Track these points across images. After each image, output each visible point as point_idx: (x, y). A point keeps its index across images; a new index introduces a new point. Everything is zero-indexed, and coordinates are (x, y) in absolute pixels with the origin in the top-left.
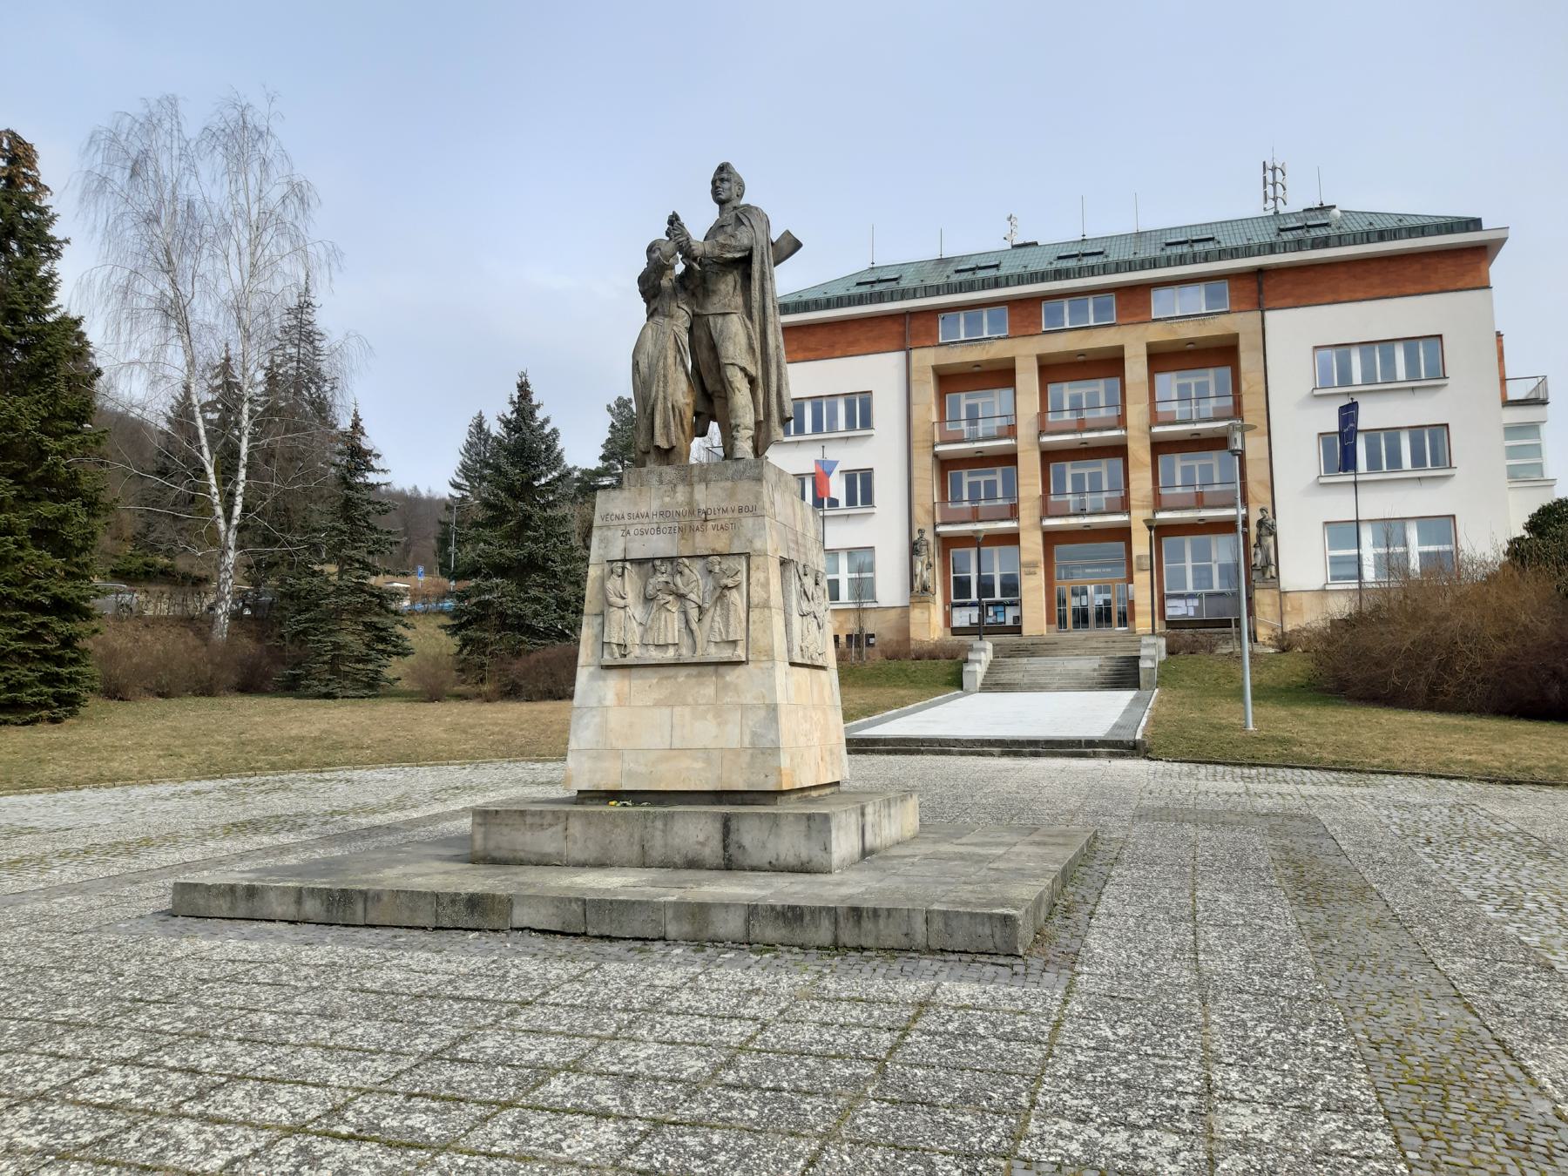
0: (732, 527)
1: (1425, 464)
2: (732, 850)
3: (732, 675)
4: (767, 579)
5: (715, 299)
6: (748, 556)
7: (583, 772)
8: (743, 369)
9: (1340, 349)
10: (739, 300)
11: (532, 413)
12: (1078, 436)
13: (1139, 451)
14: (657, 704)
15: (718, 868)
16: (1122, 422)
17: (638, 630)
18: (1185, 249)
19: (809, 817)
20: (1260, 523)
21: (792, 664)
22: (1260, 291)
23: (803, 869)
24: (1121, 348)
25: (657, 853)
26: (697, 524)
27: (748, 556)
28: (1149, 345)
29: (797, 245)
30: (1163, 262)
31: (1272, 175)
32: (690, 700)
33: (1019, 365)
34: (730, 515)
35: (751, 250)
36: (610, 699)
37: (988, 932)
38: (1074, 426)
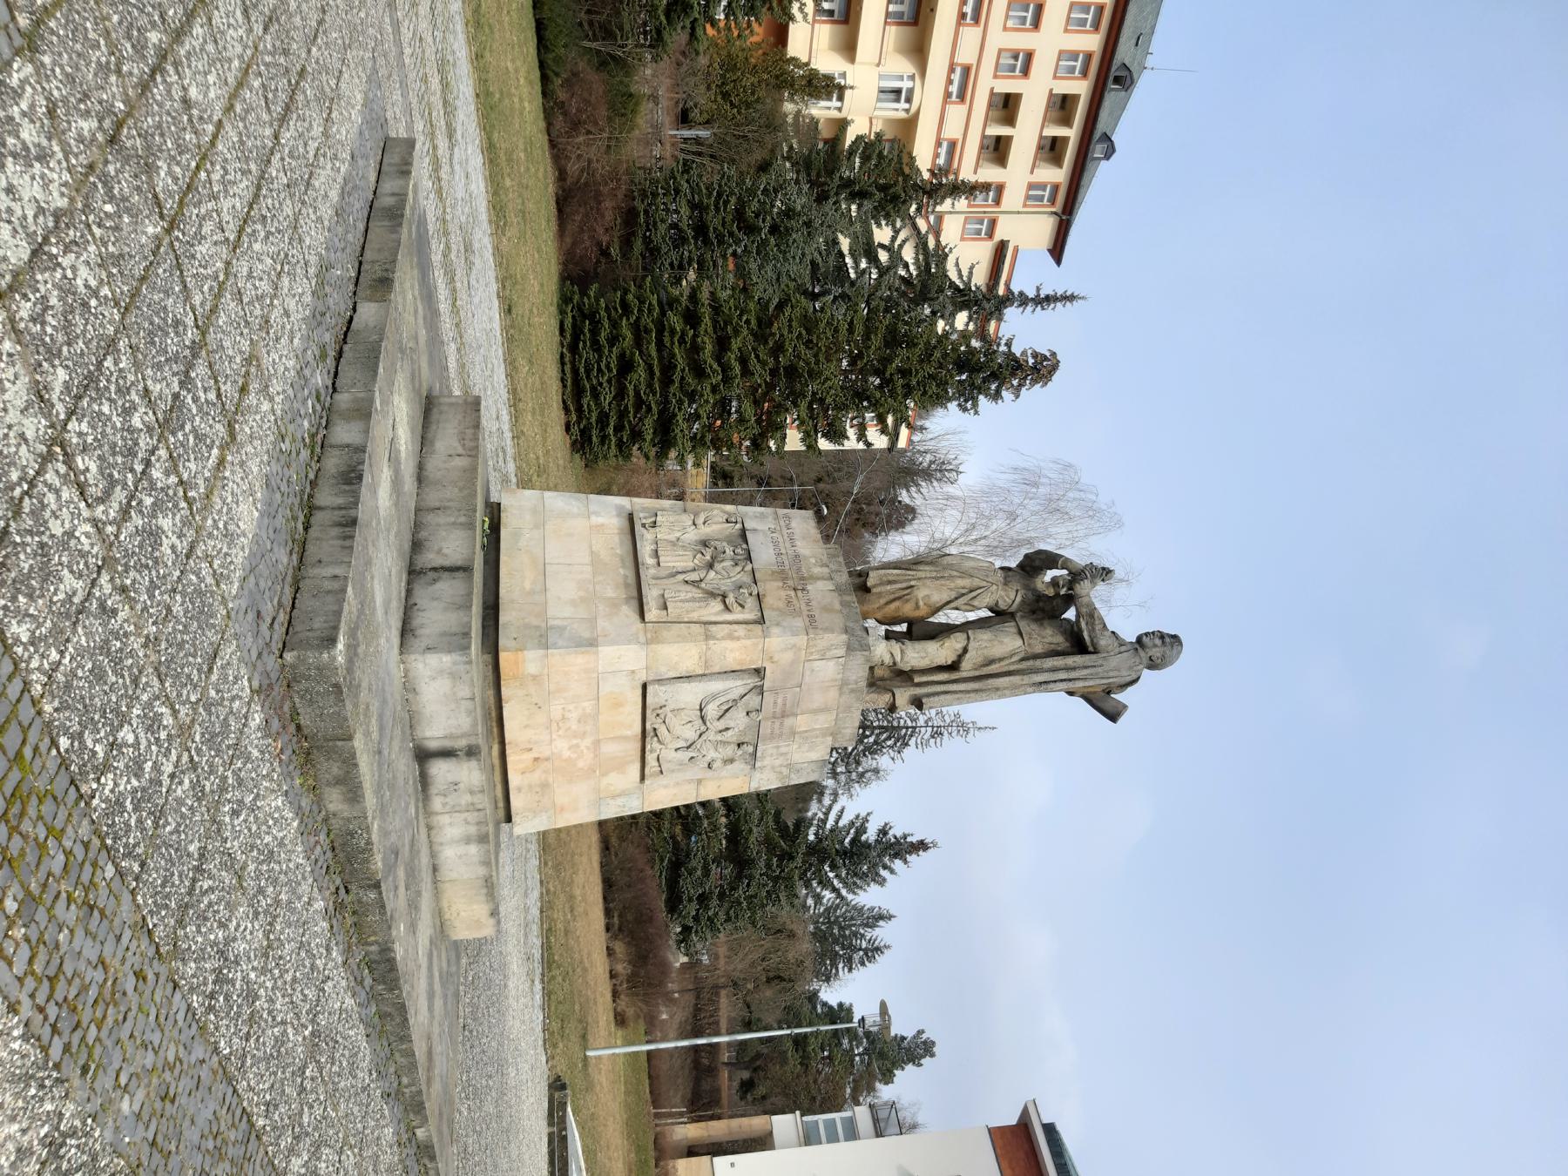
0: (790, 609)
2: (432, 575)
3: (628, 612)
4: (738, 639)
5: (1034, 626)
6: (761, 621)
7: (519, 507)
8: (965, 650)
10: (1039, 649)
11: (896, 855)
15: (411, 564)
17: (672, 537)
19: (467, 635)
21: (644, 687)
23: (406, 631)
25: (430, 518)
26: (790, 583)
27: (761, 621)
29: (1113, 716)
33: (1000, 170)
34: (804, 607)
35: (1096, 652)
36: (595, 520)
37: (316, 626)
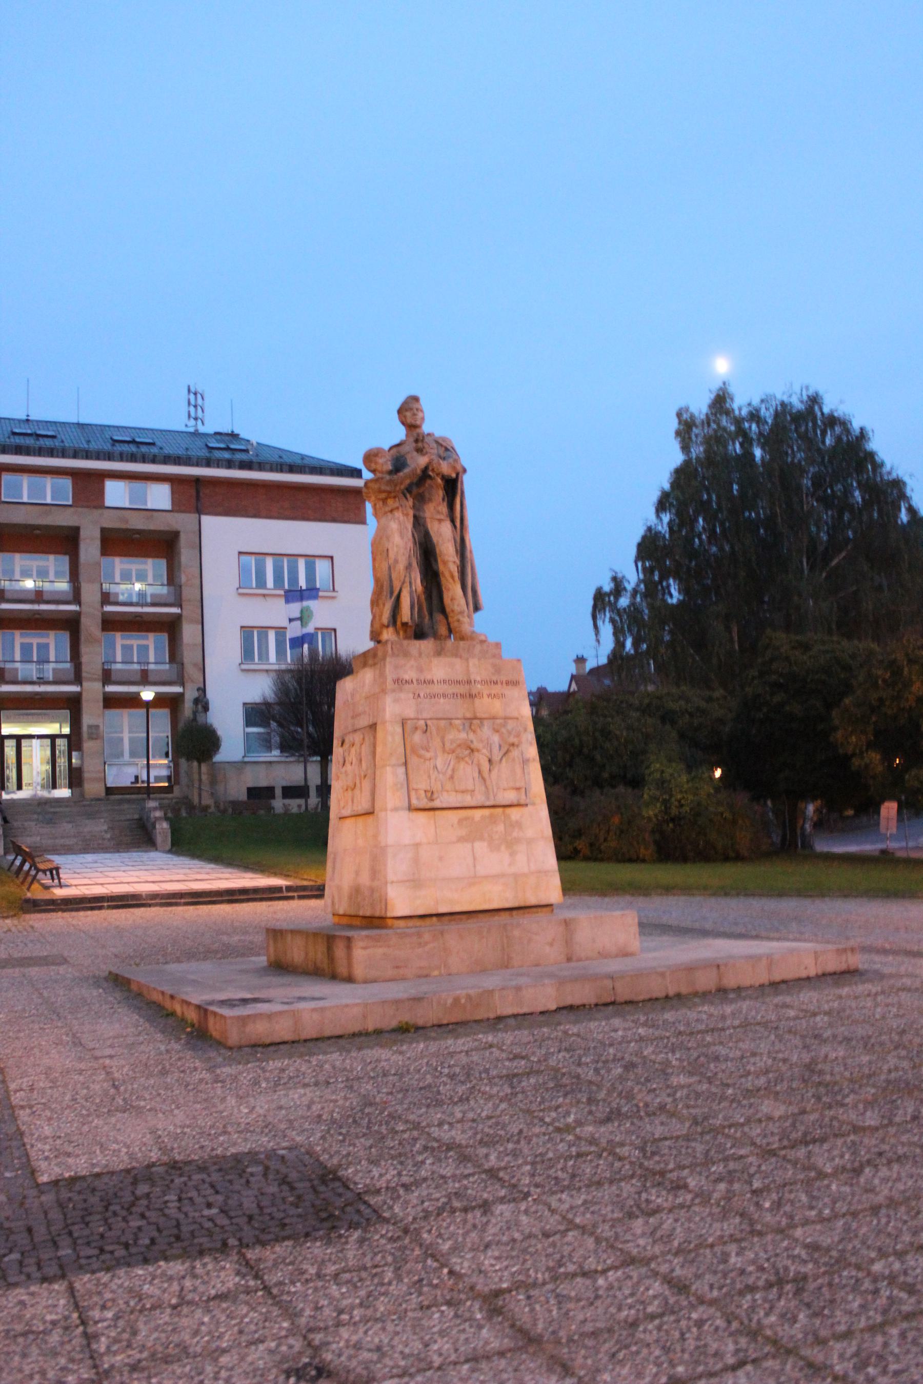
1: (253, 659)
9: (258, 557)
12: (36, 607)
13: (90, 625)
14: (461, 839)
16: (76, 598)
18: (133, 448)
20: (196, 701)
22: (198, 498)
24: (77, 530)
28: (103, 530)
30: (71, 453)
31: (195, 398)
32: (486, 835)
38: (32, 597)
